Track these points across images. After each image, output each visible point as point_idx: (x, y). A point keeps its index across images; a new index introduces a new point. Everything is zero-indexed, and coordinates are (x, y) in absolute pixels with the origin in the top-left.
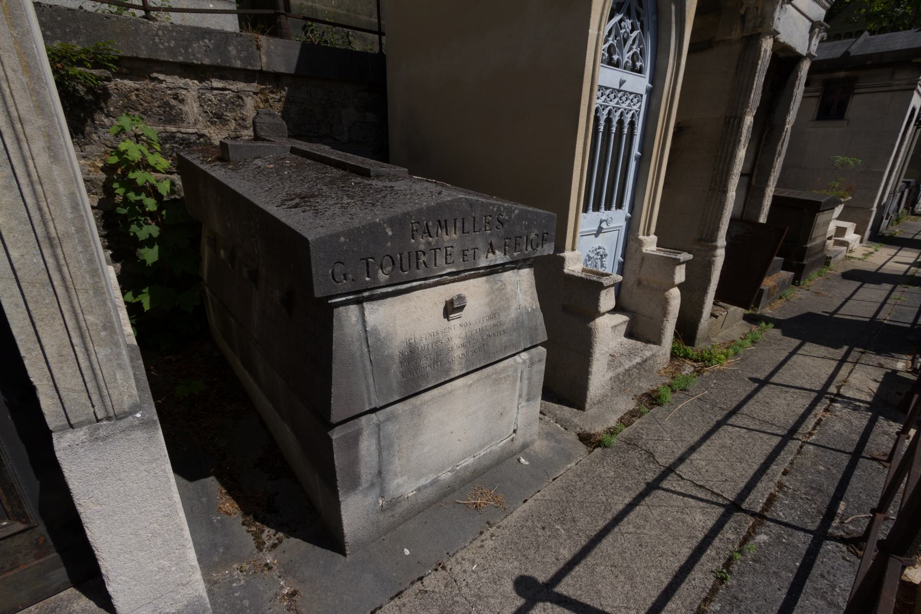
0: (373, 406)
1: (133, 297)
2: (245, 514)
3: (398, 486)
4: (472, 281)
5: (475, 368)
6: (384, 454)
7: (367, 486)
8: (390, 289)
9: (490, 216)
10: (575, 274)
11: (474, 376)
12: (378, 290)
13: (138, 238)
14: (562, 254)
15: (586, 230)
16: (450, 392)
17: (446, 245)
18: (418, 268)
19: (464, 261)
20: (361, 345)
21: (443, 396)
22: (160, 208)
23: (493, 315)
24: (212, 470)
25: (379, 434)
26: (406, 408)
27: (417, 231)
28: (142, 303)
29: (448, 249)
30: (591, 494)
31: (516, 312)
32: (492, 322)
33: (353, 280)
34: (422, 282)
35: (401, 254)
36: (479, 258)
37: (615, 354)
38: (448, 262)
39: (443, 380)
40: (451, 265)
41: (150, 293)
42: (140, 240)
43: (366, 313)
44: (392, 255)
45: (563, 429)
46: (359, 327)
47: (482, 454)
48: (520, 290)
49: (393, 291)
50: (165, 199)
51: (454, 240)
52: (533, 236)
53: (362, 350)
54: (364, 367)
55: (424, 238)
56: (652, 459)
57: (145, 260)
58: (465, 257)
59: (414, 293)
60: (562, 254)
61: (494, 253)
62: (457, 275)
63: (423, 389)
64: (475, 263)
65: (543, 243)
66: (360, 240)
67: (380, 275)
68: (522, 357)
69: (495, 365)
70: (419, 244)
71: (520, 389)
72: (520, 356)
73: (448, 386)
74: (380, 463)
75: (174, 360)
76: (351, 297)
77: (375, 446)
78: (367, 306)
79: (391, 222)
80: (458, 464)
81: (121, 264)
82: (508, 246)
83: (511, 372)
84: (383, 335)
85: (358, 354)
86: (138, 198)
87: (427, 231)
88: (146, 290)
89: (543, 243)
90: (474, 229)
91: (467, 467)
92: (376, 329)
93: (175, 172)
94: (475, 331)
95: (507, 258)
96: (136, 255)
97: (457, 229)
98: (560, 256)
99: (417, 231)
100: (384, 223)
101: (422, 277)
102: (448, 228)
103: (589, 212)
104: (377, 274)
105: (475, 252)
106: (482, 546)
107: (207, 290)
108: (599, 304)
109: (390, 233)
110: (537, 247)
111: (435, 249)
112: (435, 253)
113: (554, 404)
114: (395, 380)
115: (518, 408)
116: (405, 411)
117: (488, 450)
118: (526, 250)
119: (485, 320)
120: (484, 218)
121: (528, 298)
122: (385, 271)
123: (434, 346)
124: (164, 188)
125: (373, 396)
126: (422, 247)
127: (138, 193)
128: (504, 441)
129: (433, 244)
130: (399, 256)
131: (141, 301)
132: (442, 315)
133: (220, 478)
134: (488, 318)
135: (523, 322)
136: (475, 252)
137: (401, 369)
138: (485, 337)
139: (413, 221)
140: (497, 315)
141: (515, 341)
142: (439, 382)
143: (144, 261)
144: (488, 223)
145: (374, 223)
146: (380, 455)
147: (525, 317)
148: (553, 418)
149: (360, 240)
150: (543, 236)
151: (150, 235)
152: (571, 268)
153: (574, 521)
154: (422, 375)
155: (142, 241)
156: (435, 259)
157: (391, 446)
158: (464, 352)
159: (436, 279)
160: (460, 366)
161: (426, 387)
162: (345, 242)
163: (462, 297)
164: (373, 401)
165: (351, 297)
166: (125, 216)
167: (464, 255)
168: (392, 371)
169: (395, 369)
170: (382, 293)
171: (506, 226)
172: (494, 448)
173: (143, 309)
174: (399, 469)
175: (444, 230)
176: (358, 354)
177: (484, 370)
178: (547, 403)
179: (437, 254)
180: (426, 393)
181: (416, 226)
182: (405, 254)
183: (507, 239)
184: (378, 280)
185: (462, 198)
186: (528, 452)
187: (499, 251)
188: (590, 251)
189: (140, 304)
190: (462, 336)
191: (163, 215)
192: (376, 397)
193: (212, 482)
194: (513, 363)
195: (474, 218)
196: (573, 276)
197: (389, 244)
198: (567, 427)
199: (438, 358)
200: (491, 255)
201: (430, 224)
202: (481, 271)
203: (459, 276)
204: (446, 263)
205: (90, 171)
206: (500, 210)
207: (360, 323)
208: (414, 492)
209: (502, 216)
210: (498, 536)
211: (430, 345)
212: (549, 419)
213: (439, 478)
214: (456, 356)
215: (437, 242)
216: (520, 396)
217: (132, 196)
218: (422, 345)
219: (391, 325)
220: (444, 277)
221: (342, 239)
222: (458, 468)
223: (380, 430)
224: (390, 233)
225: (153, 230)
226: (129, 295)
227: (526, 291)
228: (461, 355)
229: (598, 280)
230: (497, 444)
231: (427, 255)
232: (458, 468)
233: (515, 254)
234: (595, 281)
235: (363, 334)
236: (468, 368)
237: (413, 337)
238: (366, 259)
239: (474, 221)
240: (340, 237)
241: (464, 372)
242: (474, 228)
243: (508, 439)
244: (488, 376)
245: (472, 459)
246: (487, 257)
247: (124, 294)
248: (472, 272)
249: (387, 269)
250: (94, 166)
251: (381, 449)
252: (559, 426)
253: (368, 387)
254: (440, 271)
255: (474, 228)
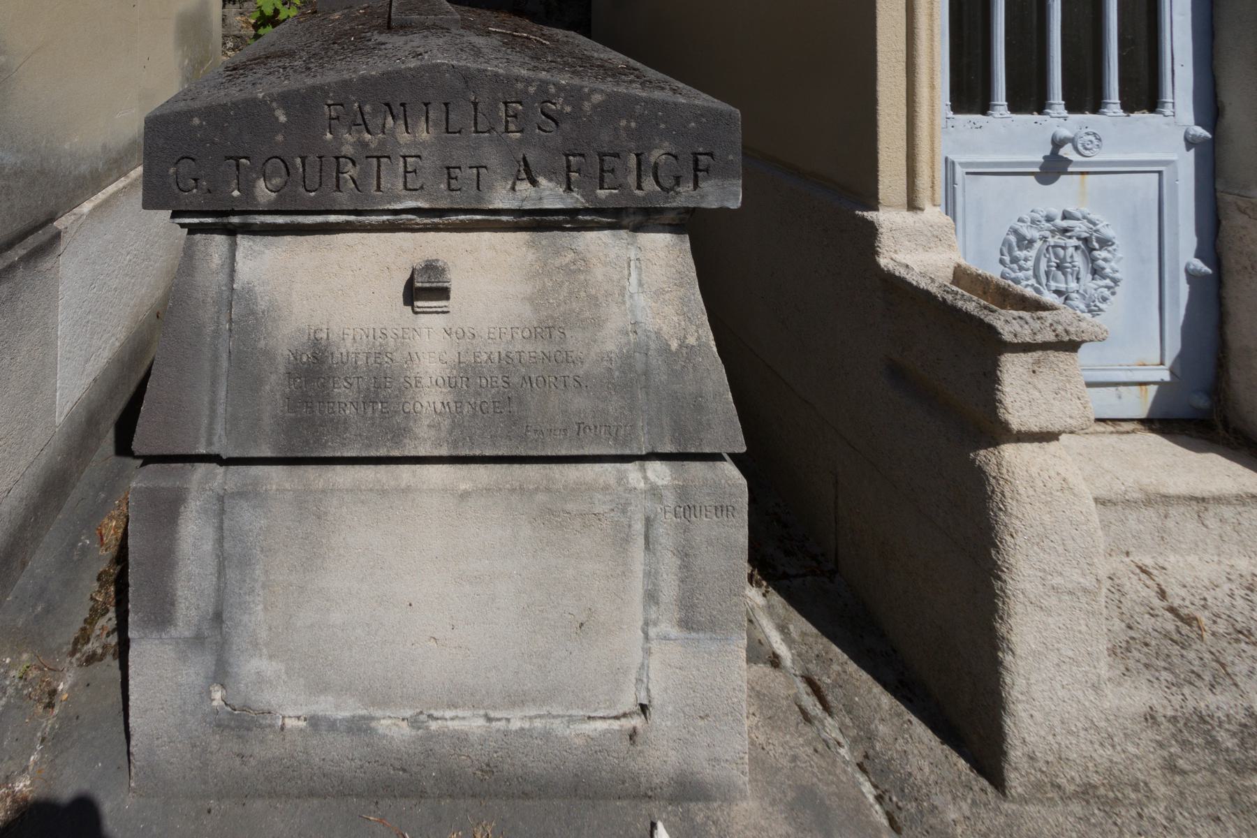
0: (215, 450)
3: (261, 680)
4: (487, 235)
5: (477, 452)
6: (232, 574)
7: (187, 634)
8: (280, 220)
9: (520, 103)
10: (909, 278)
11: (482, 473)
12: (257, 217)
14: (869, 215)
15: (987, 159)
16: (407, 490)
17: (404, 151)
18: (338, 188)
19: (450, 189)
20: (219, 312)
21: (383, 492)
23: (545, 330)
25: (221, 522)
26: (287, 486)
27: (338, 118)
29: (409, 160)
31: (624, 340)
32: (539, 348)
33: (209, 191)
34: (352, 218)
35: (303, 159)
36: (491, 188)
37: (1204, 616)
38: (409, 186)
39: (382, 452)
40: (417, 193)
43: (239, 255)
44: (285, 158)
45: (878, 815)
46: (222, 278)
47: (516, 725)
48: (640, 284)
49: (286, 225)
51: (423, 144)
52: (656, 155)
53: (218, 323)
54: (216, 358)
55: (354, 134)
57: (155, 124)
58: (453, 181)
59: (341, 236)
60: (869, 215)
61: (534, 182)
62: (440, 217)
63: (329, 453)
64: (480, 199)
65: (696, 177)
66: (226, 125)
67: (258, 190)
68: (650, 474)
69: (554, 466)
70: (342, 144)
71: (648, 574)
72: (643, 470)
73: (405, 471)
74: (221, 592)
76: (209, 220)
77: (211, 543)
78: (243, 242)
79: (285, 99)
80: (436, 714)
82: (578, 171)
83: (606, 508)
84: (262, 305)
85: (210, 329)
87: (360, 121)
89: (696, 177)
90: (447, 129)
91: (461, 739)
92: (250, 291)
94: (485, 357)
95: (575, 200)
97: (431, 123)
98: (864, 219)
99: (338, 118)
100: (271, 102)
101: (345, 208)
102: (409, 120)
103: (996, 114)
104: (254, 187)
105: (478, 173)
108: (999, 395)
109: (283, 119)
110: (678, 184)
111: (378, 158)
112: (379, 166)
113: (877, 689)
114: (269, 408)
115: (647, 637)
116: (281, 491)
117: (538, 724)
118: (639, 187)
119: (518, 336)
120: (502, 106)
121: (669, 311)
122: (268, 185)
123: (372, 360)
125: (219, 429)
126: (348, 150)
128: (600, 725)
129: (373, 146)
130: (298, 161)
132: (401, 295)
134: (526, 334)
135: (646, 373)
136: (478, 173)
137: (287, 390)
138: (515, 380)
139: (330, 102)
140: (556, 333)
141: (616, 419)
142: (373, 453)
144: (515, 116)
145: (255, 100)
146: (221, 571)
147: (656, 361)
148: (855, 741)
149: (226, 125)
150: (696, 162)
152: (901, 257)
154: (332, 420)
156: (379, 178)
157: (246, 562)
158: (449, 398)
159: (385, 218)
160: (433, 432)
161: (338, 454)
162: (201, 126)
163: (437, 268)
164: (216, 439)
165: (209, 220)
167: (450, 177)
168: (268, 387)
169: (274, 384)
170: (263, 225)
171: (566, 126)
172: (558, 727)
174: (263, 635)
175: (402, 122)
176: (210, 329)
177: (516, 468)
178: (852, 667)
179: (382, 168)
180: (349, 467)
181: (335, 110)
182: (312, 158)
183: (574, 155)
184: (254, 198)
185: (443, 64)
186: (700, 818)
187: (550, 180)
188: (1020, 220)
190: (446, 357)
192: (223, 433)
194: (612, 482)
195: (475, 104)
196: (902, 281)
197: (280, 138)
198: (900, 817)
199: (377, 394)
200: (524, 186)
201: (367, 108)
202: (504, 218)
203: (445, 219)
204: (406, 188)
205: (242, 27)
206: (546, 92)
207: (227, 270)
208: (302, 724)
209: (554, 104)
211: (362, 357)
212: (836, 734)
213: (373, 724)
214: (425, 404)
215: (382, 144)
216: (651, 597)
218: (344, 351)
219: (283, 289)
220: (404, 216)
221: (196, 121)
222: (434, 726)
223: (222, 511)
224: (283, 119)
227: (659, 293)
228: (439, 406)
229: (983, 315)
230: (571, 719)
231: (358, 167)
232: (434, 726)
233: (602, 193)
234: (968, 316)
235: (226, 294)
236: (455, 444)
237: (324, 327)
238: (237, 159)
239: (476, 109)
240: (192, 117)
241: (444, 451)
242: (476, 124)
243: (616, 725)
244: (521, 490)
245: (482, 722)
246: (513, 189)
248: (478, 217)
249: (274, 182)
250: (247, 22)
251: (224, 559)
252: (868, 789)
253: (213, 403)
254: (389, 203)
255: (476, 124)
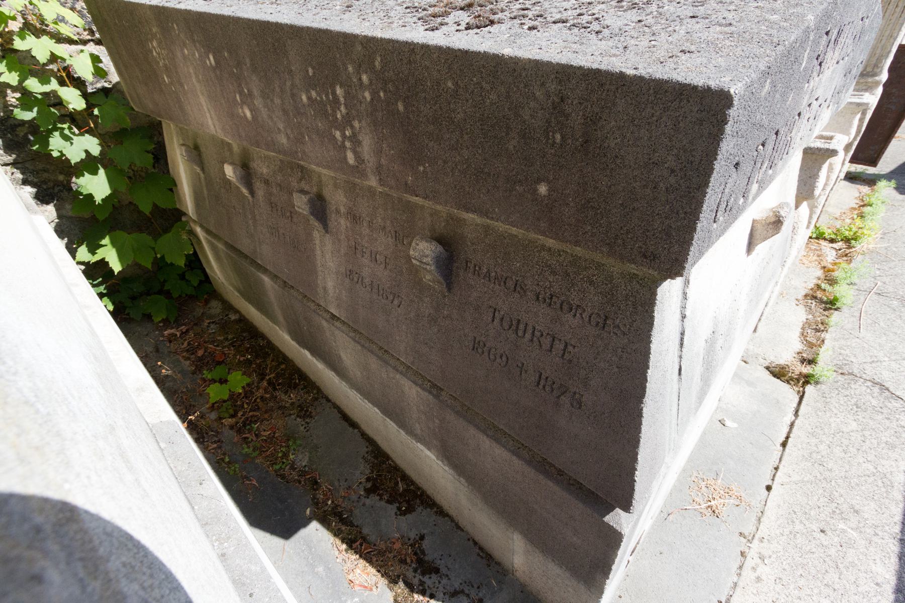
1: (90, 254)
2: (390, 582)
13: (68, 160)
22: (90, 106)
24: (81, 197)
28: (107, 263)
30: (849, 462)
41: (114, 243)
42: (73, 162)
50: (74, 179)
56: (887, 393)
75: (178, 334)
81: (55, 206)
86: (47, 88)
88: (106, 241)
93: (89, 41)
96: (71, 189)
106: (759, 579)
107: (198, 230)
124: (83, 68)
127: (44, 81)
131: (103, 260)
133: (324, 522)
143: (90, 197)
151: (87, 152)
153: (857, 512)
155: (76, 164)
166: (32, 126)
173: (112, 271)
189: (103, 263)
191: (97, 116)
193: (315, 532)
210: (770, 557)
217: (33, 85)
225: (92, 144)
226: (83, 253)
247: (73, 253)
